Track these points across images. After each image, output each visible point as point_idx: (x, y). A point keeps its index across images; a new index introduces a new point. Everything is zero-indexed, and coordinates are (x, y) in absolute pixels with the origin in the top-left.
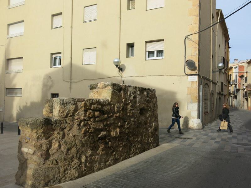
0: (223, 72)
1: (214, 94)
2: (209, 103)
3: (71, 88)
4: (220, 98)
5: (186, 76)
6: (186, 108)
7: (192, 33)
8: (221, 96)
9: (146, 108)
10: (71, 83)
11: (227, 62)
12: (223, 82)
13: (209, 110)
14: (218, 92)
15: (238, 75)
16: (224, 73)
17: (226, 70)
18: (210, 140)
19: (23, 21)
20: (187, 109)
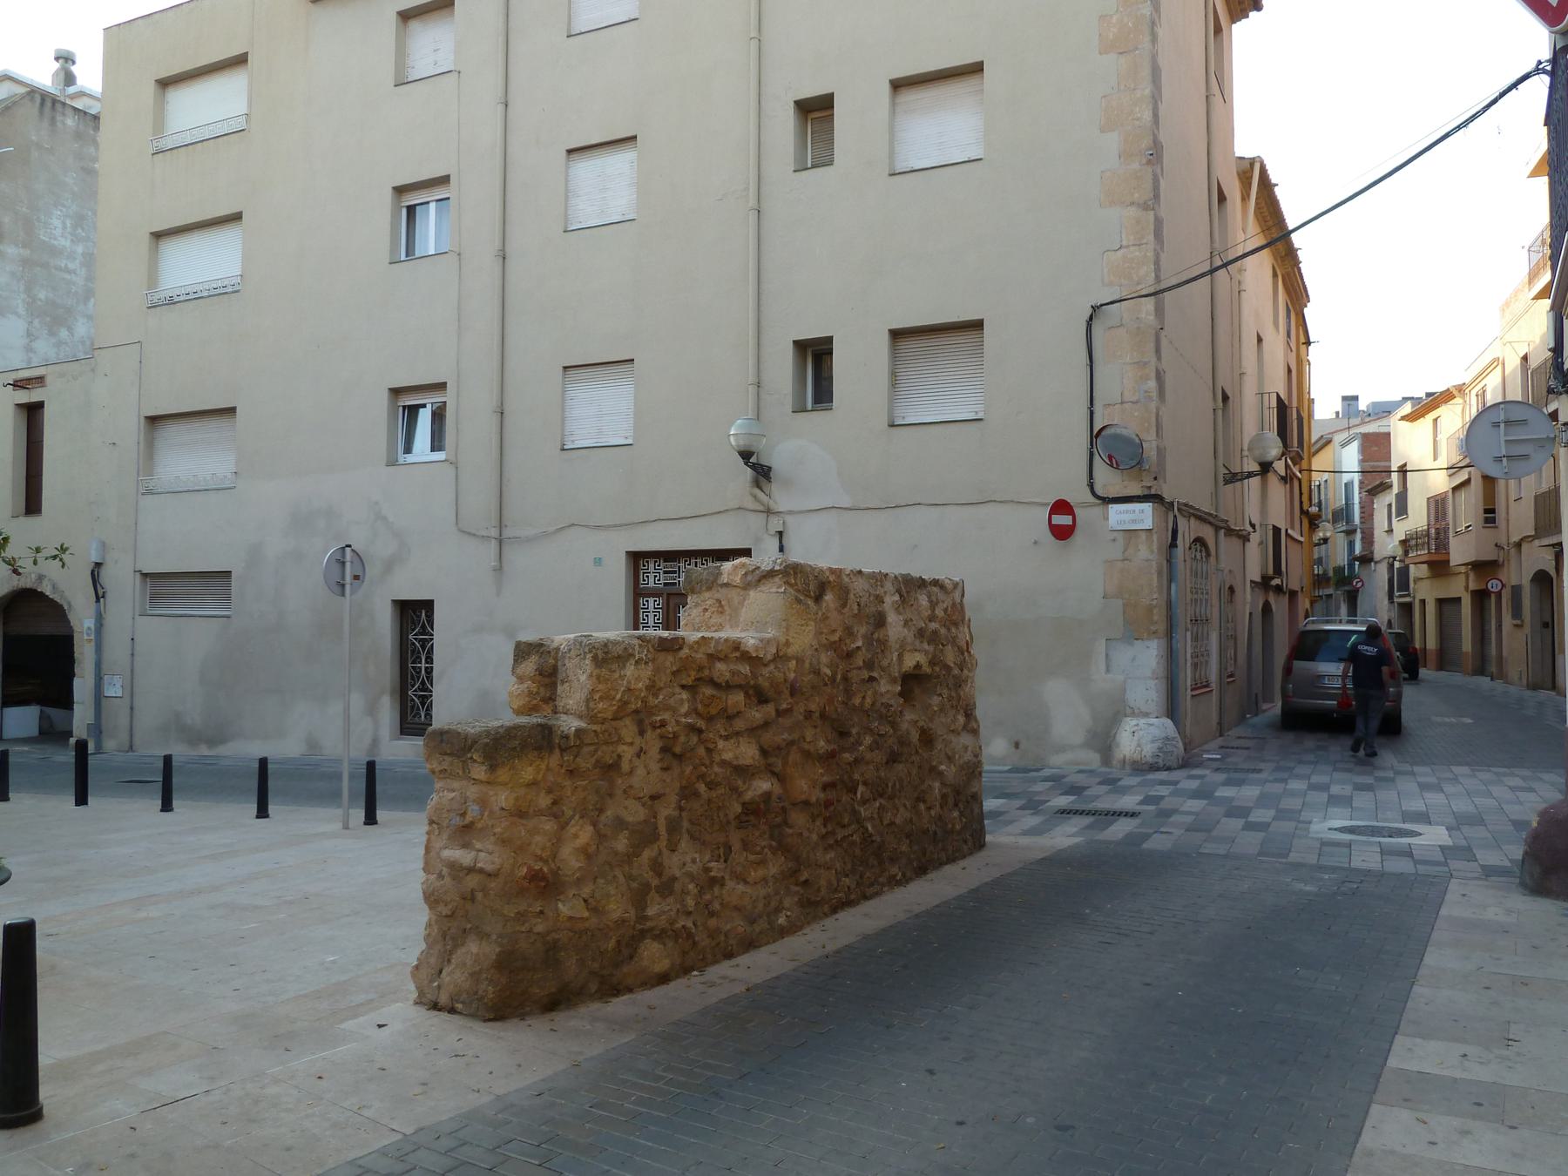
0: (1283, 473)
1: (1238, 590)
2: (1214, 637)
3: (499, 569)
4: (1267, 609)
5: (1095, 505)
6: (1103, 667)
7: (1124, 294)
8: (1272, 598)
9: (926, 669)
10: (501, 542)
11: (1300, 419)
12: (1282, 525)
13: (1213, 676)
14: (1258, 579)
15: (1361, 482)
16: (1284, 479)
17: (1297, 459)
18: (1224, 820)
19: (236, 217)
20: (1108, 670)
